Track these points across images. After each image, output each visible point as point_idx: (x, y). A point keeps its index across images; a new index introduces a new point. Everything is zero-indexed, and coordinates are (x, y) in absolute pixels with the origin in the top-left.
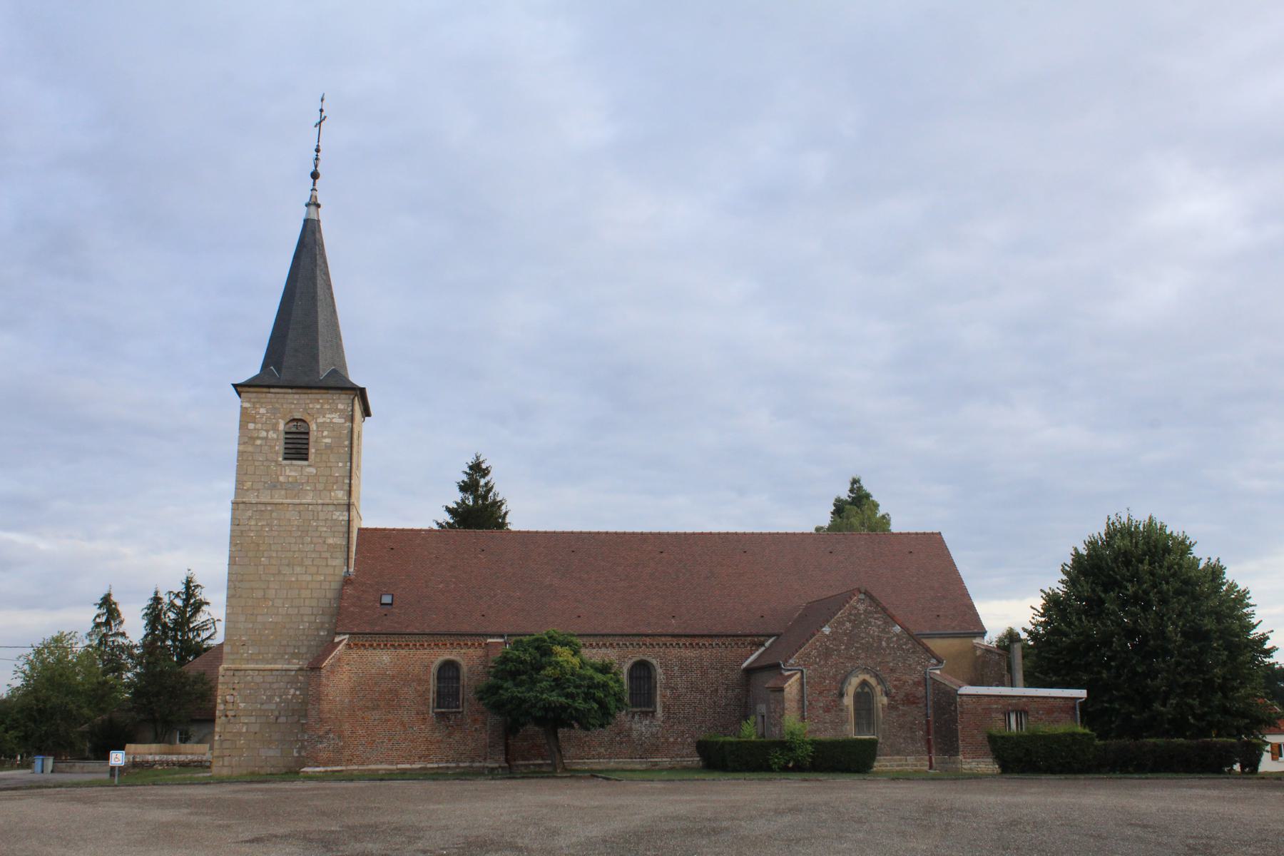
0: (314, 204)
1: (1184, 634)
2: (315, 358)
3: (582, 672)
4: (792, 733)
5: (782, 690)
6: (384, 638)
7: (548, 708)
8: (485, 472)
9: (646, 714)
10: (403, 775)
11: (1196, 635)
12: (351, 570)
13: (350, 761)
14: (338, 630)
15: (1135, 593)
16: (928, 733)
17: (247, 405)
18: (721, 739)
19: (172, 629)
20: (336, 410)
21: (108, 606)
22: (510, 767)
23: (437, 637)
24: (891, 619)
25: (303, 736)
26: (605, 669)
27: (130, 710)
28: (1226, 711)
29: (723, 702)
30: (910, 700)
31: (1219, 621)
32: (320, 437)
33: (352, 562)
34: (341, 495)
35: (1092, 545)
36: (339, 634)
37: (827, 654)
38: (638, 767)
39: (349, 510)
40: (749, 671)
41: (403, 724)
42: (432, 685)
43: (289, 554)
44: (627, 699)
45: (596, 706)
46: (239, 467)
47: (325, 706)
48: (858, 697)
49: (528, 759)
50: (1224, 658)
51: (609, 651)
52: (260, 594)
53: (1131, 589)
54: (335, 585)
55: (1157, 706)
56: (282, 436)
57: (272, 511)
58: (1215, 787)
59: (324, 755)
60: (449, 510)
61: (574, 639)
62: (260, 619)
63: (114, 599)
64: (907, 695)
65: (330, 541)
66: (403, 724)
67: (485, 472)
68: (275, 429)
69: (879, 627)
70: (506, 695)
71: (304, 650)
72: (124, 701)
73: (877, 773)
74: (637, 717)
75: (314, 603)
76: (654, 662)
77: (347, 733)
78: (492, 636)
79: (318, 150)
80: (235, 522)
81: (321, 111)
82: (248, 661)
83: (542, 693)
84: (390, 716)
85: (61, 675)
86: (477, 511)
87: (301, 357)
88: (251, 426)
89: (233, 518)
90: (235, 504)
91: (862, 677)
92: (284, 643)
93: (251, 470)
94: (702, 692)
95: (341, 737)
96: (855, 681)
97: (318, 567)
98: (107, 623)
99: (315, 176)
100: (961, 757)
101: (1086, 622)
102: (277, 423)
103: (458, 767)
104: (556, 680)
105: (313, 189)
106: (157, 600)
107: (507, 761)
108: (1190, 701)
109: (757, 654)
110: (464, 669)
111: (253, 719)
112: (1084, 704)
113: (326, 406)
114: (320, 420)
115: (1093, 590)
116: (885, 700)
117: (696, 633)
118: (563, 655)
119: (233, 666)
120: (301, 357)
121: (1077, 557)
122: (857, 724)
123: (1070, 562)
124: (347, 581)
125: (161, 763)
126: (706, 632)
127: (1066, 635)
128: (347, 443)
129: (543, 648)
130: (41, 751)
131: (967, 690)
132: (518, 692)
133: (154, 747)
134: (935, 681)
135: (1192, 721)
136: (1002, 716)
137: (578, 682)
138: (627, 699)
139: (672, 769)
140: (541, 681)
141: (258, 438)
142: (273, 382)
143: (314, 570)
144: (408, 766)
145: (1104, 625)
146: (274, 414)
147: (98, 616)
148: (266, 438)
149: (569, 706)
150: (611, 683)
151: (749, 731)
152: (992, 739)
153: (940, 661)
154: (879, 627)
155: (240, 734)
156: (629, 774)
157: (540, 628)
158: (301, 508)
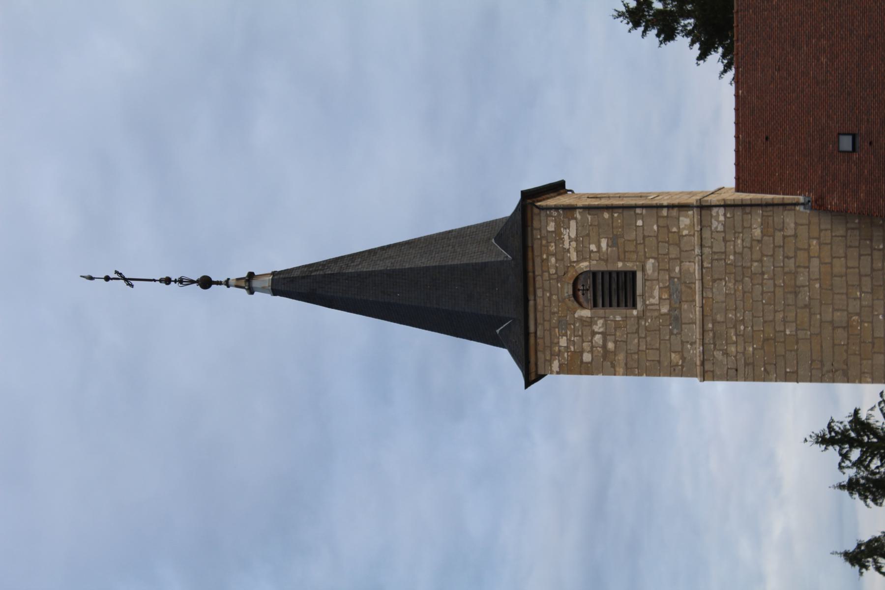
0: (249, 283)
12: (801, 199)
17: (556, 365)
20: (558, 233)
33: (789, 198)
34: (685, 221)
39: (710, 207)
43: (779, 293)
52: (841, 334)
56: (601, 312)
57: (714, 322)
60: (702, 56)
63: (851, 547)
65: (757, 233)
68: (591, 322)
79: (167, 281)
80: (732, 374)
81: (107, 279)
88: (587, 357)
89: (727, 377)
97: (797, 249)
102: (581, 319)
106: (852, 486)
113: (552, 248)
114: (574, 256)
124: (818, 205)
128: (606, 215)
141: (604, 346)
143: (802, 255)
148: (604, 335)
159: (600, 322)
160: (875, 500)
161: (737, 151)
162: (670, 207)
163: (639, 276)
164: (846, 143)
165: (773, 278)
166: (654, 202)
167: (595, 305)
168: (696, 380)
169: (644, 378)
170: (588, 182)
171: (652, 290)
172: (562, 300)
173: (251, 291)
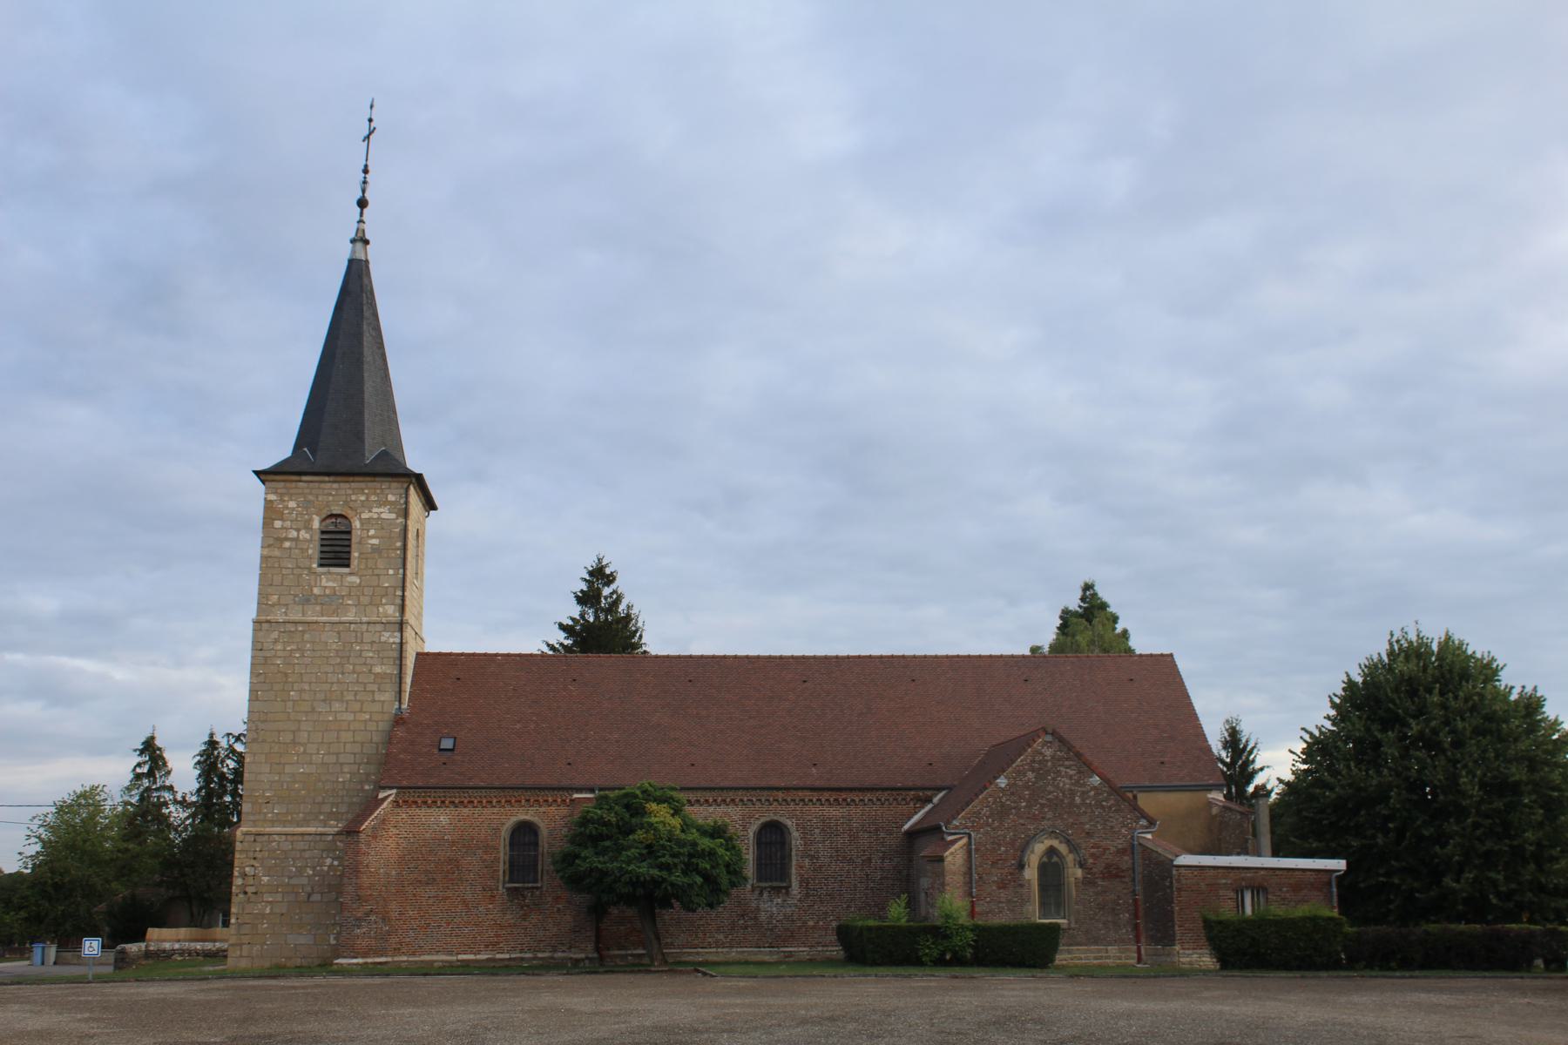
0: (361, 240)
1: (1483, 785)
2: (359, 437)
3: (683, 836)
4: (948, 916)
5: (941, 859)
6: (441, 793)
7: (636, 882)
8: (609, 580)
9: (777, 890)
10: (465, 968)
11: (1500, 787)
12: (405, 706)
13: (397, 951)
14: (383, 783)
15: (1421, 733)
16: (1136, 916)
17: (272, 497)
18: (860, 923)
19: (232, 781)
20: (386, 503)
21: (150, 749)
22: (601, 958)
23: (510, 792)
24: (1088, 768)
25: (343, 921)
26: (717, 832)
27: (159, 884)
28: (1542, 888)
29: (878, 875)
30: (1112, 873)
31: (1532, 768)
32: (367, 531)
33: (406, 696)
34: (391, 611)
35: (1372, 669)
36: (384, 788)
37: (1002, 812)
38: (767, 958)
39: (401, 631)
40: (912, 835)
41: (465, 903)
42: (503, 853)
43: (326, 687)
44: (750, 870)
45: (699, 880)
46: (263, 577)
47: (365, 880)
48: (1043, 868)
49: (624, 948)
50: (1540, 819)
51: (730, 809)
52: (288, 737)
53: (1415, 727)
54: (384, 726)
55: (1448, 881)
56: (317, 536)
57: (303, 632)
58: (1441, 991)
59: (362, 943)
60: (562, 627)
61: (674, 794)
62: (288, 769)
63: (158, 743)
64: (1108, 866)
65: (378, 669)
66: (465, 903)
67: (609, 580)
68: (308, 528)
69: (1071, 777)
70: (583, 866)
71: (343, 809)
72: (133, 876)
73: (1058, 968)
74: (765, 895)
75: (357, 749)
76: (789, 823)
77: (394, 915)
78: (580, 790)
79: (366, 171)
80: (257, 647)
81: (370, 120)
82: (273, 823)
83: (629, 863)
84: (449, 894)
85: (85, 841)
86: (602, 629)
87: (346, 436)
88: (278, 524)
89: (255, 642)
90: (258, 623)
91: (1048, 843)
92: (319, 799)
93: (277, 579)
94: (851, 861)
95: (385, 919)
96: (1039, 848)
97: (362, 703)
98: (151, 774)
99: (362, 203)
100: (1177, 948)
101: (1355, 771)
102: (311, 520)
103: (535, 958)
104: (649, 847)
105: (361, 221)
106: (212, 744)
107: (597, 950)
108: (1492, 875)
109: (922, 812)
110: (544, 832)
111: (279, 897)
112: (1342, 878)
113: (373, 498)
114: (364, 516)
115: (1368, 730)
116: (1079, 873)
117: (843, 785)
118: (660, 814)
119: (253, 830)
120: (346, 436)
121: (1350, 685)
122: (1043, 904)
123: (1340, 692)
124: (398, 720)
125: (182, 952)
126: (856, 785)
127: (1332, 789)
128: (399, 544)
129: (633, 807)
130: (34, 939)
131: (1186, 860)
132: (598, 862)
133: (183, 932)
134: (1145, 849)
135: (1494, 901)
136: (1232, 895)
137: (676, 849)
138: (750, 870)
139: (812, 962)
140: (629, 848)
141: (286, 539)
142: (305, 468)
143: (357, 706)
144: (471, 957)
145: (1379, 773)
146: (307, 508)
147: (139, 765)
148: (296, 540)
149: (664, 880)
150: (721, 851)
151: (897, 912)
152: (1208, 924)
153: (1152, 823)
154: (1071, 777)
155: (263, 916)
156: (722, 969)
157: (634, 781)
158: (341, 627)
159: (308, 536)
160: (199, 763)
161: (450, 654)
162: (403, 598)
163: (346, 570)
164: (447, 743)
165: (339, 682)
166: (408, 584)
167: (323, 532)
168: (254, 615)
169: (257, 572)
170: (436, 531)
171: (334, 581)
172: (328, 505)
173: (353, 241)
